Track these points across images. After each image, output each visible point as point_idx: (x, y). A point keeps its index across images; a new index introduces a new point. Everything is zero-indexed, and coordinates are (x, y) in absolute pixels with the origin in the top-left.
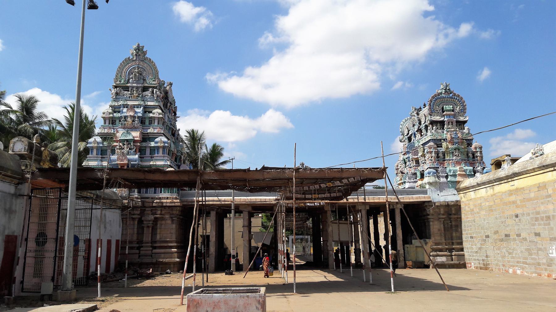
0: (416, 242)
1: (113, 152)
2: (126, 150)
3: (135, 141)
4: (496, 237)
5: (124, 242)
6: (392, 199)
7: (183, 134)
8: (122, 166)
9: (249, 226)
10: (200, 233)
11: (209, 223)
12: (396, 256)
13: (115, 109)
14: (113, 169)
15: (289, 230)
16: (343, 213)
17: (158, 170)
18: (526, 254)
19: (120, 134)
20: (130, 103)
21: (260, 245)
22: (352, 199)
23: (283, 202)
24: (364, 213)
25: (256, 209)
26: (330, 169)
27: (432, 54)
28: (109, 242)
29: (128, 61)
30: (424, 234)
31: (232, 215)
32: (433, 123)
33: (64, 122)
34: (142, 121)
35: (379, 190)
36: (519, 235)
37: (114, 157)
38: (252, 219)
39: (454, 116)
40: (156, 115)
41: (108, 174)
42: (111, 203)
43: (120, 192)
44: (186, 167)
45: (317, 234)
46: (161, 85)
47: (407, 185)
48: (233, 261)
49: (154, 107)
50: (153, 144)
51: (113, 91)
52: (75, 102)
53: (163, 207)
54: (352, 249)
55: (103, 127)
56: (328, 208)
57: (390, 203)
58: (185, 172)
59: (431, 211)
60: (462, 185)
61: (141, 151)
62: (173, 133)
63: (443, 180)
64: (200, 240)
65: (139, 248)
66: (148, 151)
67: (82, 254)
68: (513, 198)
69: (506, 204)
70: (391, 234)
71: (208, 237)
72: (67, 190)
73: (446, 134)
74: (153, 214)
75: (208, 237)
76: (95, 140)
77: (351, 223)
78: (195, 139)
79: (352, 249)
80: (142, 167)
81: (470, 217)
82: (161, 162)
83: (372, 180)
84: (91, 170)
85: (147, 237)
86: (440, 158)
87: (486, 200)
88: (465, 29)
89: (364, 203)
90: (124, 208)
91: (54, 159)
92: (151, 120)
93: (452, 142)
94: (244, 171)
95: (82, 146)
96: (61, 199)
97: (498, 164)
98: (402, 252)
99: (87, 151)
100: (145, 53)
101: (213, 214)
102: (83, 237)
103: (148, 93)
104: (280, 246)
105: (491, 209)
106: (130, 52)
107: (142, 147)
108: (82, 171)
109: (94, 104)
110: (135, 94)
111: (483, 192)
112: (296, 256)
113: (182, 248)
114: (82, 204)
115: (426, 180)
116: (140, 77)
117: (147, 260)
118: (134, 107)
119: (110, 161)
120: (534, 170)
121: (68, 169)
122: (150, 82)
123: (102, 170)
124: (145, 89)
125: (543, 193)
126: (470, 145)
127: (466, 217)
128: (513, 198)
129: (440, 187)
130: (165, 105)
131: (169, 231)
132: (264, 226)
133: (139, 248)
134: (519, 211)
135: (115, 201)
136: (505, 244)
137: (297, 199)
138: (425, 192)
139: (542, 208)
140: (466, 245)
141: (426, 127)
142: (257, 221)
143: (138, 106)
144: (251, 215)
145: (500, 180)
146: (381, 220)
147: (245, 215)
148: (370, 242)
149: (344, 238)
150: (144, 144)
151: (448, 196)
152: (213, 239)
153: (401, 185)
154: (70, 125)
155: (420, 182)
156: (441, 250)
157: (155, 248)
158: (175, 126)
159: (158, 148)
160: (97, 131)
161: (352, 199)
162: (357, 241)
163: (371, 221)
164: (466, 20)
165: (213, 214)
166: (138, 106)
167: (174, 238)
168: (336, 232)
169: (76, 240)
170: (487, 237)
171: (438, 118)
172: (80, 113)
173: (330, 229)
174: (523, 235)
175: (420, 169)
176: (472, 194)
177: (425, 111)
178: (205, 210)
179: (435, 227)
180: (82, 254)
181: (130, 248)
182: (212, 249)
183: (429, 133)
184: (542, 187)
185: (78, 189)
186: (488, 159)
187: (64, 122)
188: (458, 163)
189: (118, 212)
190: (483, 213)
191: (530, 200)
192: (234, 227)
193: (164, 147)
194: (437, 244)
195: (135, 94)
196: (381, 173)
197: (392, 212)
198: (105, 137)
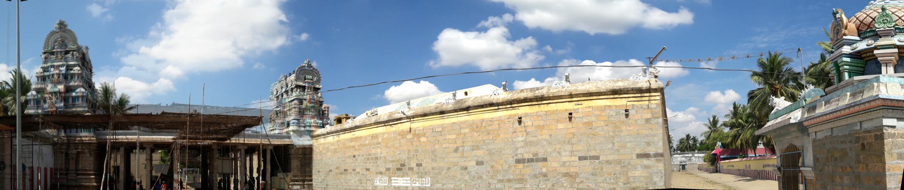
0: (280, 175)
1: (45, 102)
2: (54, 99)
3: (60, 93)
4: (337, 171)
5: (56, 170)
6: (265, 141)
7: (98, 86)
8: (52, 112)
9: (151, 160)
10: (112, 164)
11: (119, 157)
12: (265, 185)
13: (45, 69)
14: (46, 115)
15: (183, 164)
16: (226, 150)
17: (79, 115)
18: (358, 183)
19: (50, 88)
20: (56, 64)
21: (159, 175)
22: (234, 140)
23: (180, 141)
24: (243, 151)
25: (157, 146)
26: (217, 115)
27: (282, 49)
28: (46, 169)
29: (53, 33)
30: (286, 169)
31: (137, 151)
32: (298, 87)
33: (10, 83)
34: (66, 76)
35: (257, 135)
36: (354, 170)
37: (46, 106)
38: (153, 155)
39: (313, 83)
40: (76, 72)
41: (42, 119)
42: (46, 140)
43: (51, 132)
44: (100, 112)
45: (205, 167)
46: (79, 49)
47: (277, 132)
48: (138, 187)
49: (74, 66)
50: (74, 94)
51: (43, 56)
52: (16, 67)
53: (83, 143)
54: (232, 179)
55: (37, 84)
56: (215, 147)
57: (263, 145)
58: (100, 116)
59: (292, 151)
60: (316, 133)
61: (65, 100)
62: (90, 86)
63: (302, 129)
64: (112, 170)
65: (66, 174)
66: (70, 100)
67: (28, 177)
68: (353, 144)
69: (347, 148)
70: (262, 168)
71: (118, 167)
72: (15, 132)
73: (307, 96)
74: (76, 149)
75: (118, 167)
76: (32, 93)
77: (232, 159)
78: (107, 92)
79: (232, 179)
80: (67, 113)
81: (319, 157)
82: (81, 108)
83: (251, 126)
84: (30, 116)
85: (72, 166)
86: (302, 113)
87: (332, 144)
88: (304, 36)
89: (244, 144)
90: (54, 144)
91: (6, 109)
92: (73, 76)
93: (310, 102)
94: (147, 115)
95: (23, 98)
96: (13, 137)
97: (339, 121)
98: (269, 182)
99: (27, 102)
100: (65, 26)
101: (122, 149)
102: (28, 165)
103: (69, 55)
104: (175, 176)
105: (335, 151)
106: (54, 26)
107: (66, 96)
108: (25, 117)
109: (30, 67)
110: (60, 57)
111: (330, 139)
112: (188, 184)
113: (99, 175)
114: (26, 141)
115: (291, 128)
116: (63, 44)
117: (73, 183)
118: (59, 66)
119: (43, 109)
120: (370, 125)
121: (15, 116)
122: (71, 46)
123: (37, 115)
124: (67, 52)
125: (375, 141)
126: (321, 105)
127: (316, 157)
128: (353, 144)
129: (299, 134)
130: (83, 64)
131: (88, 162)
132: (163, 160)
133: (66, 174)
134: (356, 153)
135: (48, 139)
136: (343, 176)
137: (190, 139)
138: (289, 137)
139: (373, 151)
140: (314, 177)
141: (292, 89)
142: (157, 156)
143: (62, 66)
144: (152, 151)
145: (345, 131)
146: (255, 158)
147: (148, 150)
148: (246, 175)
149: (226, 171)
150: (67, 95)
151: (304, 141)
152: (122, 169)
153: (269, 132)
154: (15, 84)
155: (285, 130)
156: (297, 181)
157: (78, 174)
158: (91, 80)
159: (78, 97)
160: (33, 86)
161: (234, 140)
162: (236, 174)
163: (248, 158)
164: (304, 31)
165: (122, 149)
166: (62, 66)
167: (92, 167)
168: (220, 165)
169: (24, 167)
170: (331, 171)
171: (301, 84)
172: (20, 75)
173: (216, 164)
174: (358, 170)
175: (287, 119)
176: (322, 140)
177: (293, 77)
178: (116, 146)
179: (295, 163)
180: (28, 177)
181: (61, 174)
182: (122, 177)
183: (294, 94)
184: (374, 137)
185: (23, 130)
186: (332, 116)
187: (10, 83)
188: (313, 117)
189: (51, 147)
190: (329, 154)
191: (366, 145)
192: (138, 160)
193: (83, 97)
194: (295, 176)
195: (60, 57)
196: (257, 121)
197: (265, 151)
198: (39, 91)
